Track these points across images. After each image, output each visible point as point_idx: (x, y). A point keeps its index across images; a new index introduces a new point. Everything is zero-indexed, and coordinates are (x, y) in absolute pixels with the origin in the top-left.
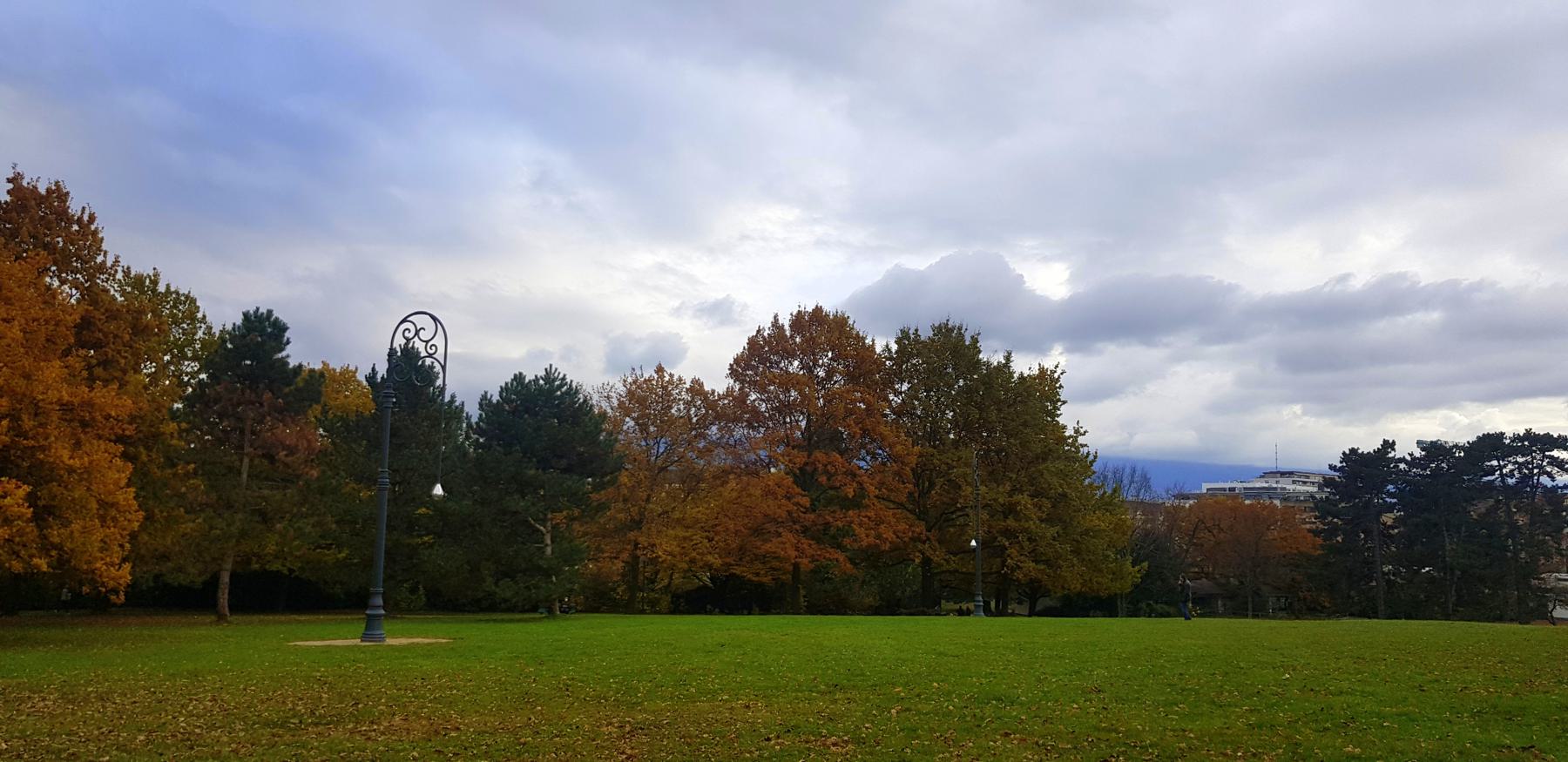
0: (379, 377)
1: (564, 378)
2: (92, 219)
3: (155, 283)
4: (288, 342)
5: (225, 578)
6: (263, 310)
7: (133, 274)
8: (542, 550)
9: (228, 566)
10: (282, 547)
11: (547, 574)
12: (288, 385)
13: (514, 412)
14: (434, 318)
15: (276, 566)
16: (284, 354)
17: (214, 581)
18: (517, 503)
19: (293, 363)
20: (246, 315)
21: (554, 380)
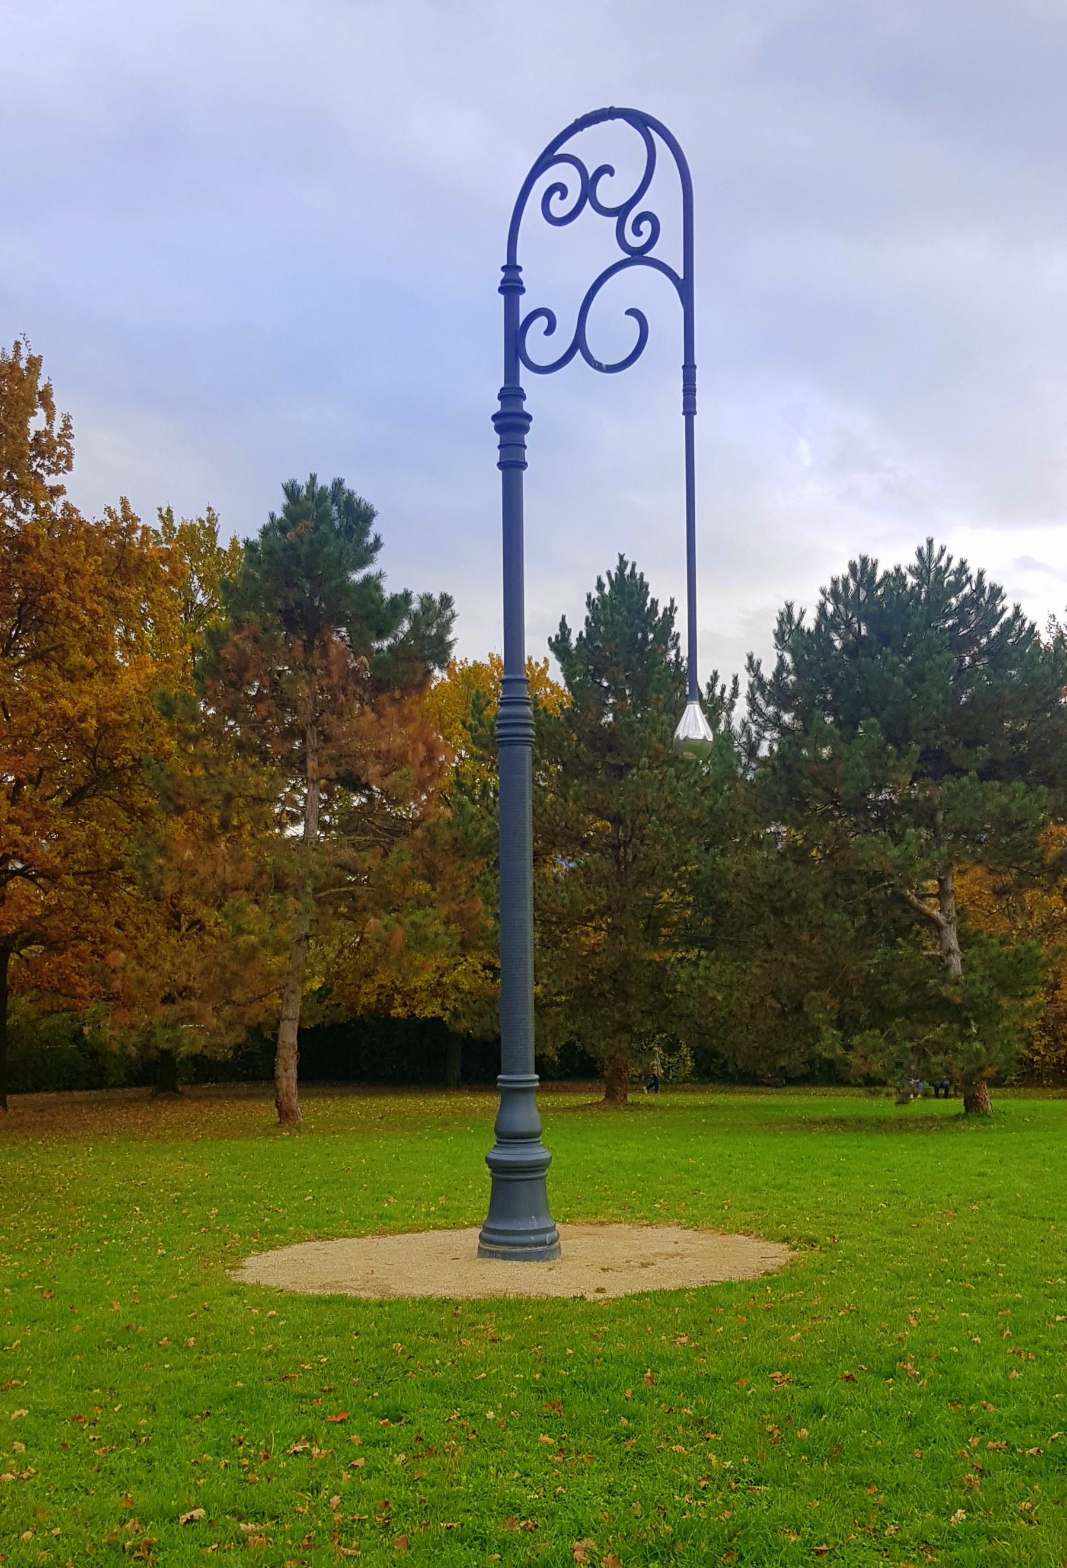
0: (573, 641)
1: (963, 567)
2: (34, 363)
3: (212, 533)
4: (377, 545)
5: (289, 1036)
6: (325, 481)
7: (177, 524)
8: (941, 964)
9: (293, 1011)
10: (430, 975)
11: (957, 1014)
12: (381, 635)
13: (855, 648)
14: (641, 122)
15: (431, 1010)
16: (371, 570)
17: (271, 1048)
18: (875, 851)
19: (390, 589)
20: (291, 491)
21: (940, 572)
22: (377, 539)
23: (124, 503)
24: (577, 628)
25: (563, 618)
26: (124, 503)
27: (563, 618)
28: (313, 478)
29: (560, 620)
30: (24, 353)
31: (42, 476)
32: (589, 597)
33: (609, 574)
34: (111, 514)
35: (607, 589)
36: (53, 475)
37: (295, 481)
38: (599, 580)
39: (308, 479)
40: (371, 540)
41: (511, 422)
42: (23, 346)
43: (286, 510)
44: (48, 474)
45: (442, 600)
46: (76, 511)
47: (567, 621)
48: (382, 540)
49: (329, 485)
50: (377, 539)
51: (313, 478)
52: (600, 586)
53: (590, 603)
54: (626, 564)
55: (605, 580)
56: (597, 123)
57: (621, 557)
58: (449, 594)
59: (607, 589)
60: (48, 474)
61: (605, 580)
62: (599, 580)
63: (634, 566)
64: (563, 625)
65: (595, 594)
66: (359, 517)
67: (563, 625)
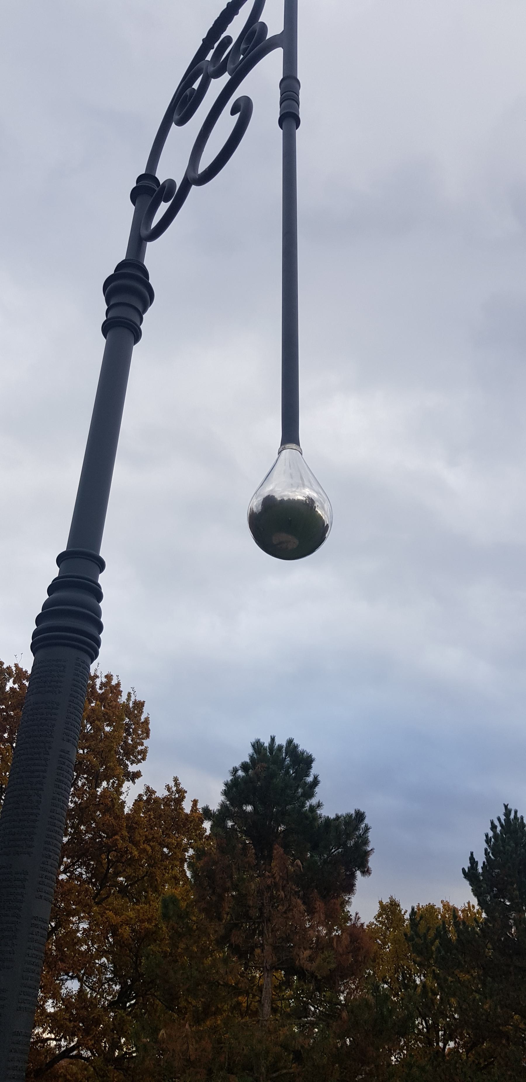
4: (316, 782)
6: (281, 741)
22: (316, 778)
23: (176, 780)
24: (481, 859)
25: (472, 854)
26: (176, 780)
27: (472, 854)
28: (273, 739)
29: (470, 855)
30: (133, 699)
31: (127, 765)
32: (487, 836)
33: (499, 819)
34: (169, 788)
35: (499, 829)
36: (134, 765)
37: (259, 740)
38: (492, 823)
39: (269, 740)
40: (310, 779)
41: (128, 294)
42: (132, 695)
43: (252, 757)
44: (132, 764)
45: (356, 816)
46: (154, 792)
47: (474, 856)
48: (319, 778)
49: (284, 743)
50: (316, 778)
51: (273, 739)
52: (493, 827)
53: (488, 841)
54: (510, 811)
55: (497, 823)
56: (216, 22)
57: (506, 807)
58: (362, 810)
59: (499, 829)
60: (132, 764)
61: (497, 823)
62: (492, 823)
63: (516, 812)
64: (472, 859)
65: (491, 834)
66: (303, 762)
67: (472, 859)
